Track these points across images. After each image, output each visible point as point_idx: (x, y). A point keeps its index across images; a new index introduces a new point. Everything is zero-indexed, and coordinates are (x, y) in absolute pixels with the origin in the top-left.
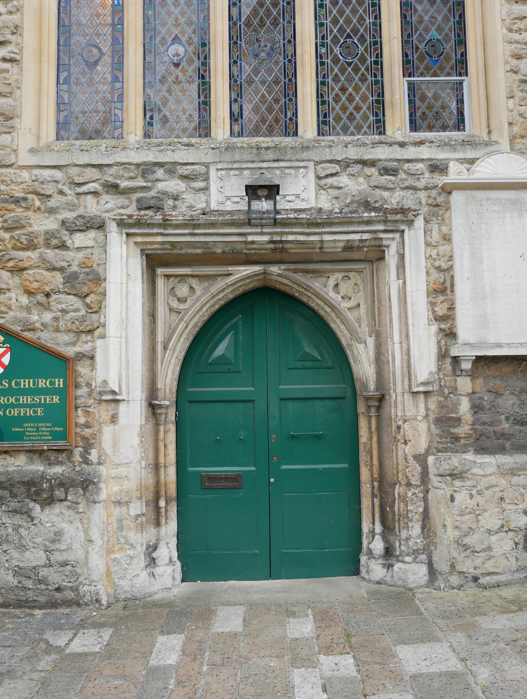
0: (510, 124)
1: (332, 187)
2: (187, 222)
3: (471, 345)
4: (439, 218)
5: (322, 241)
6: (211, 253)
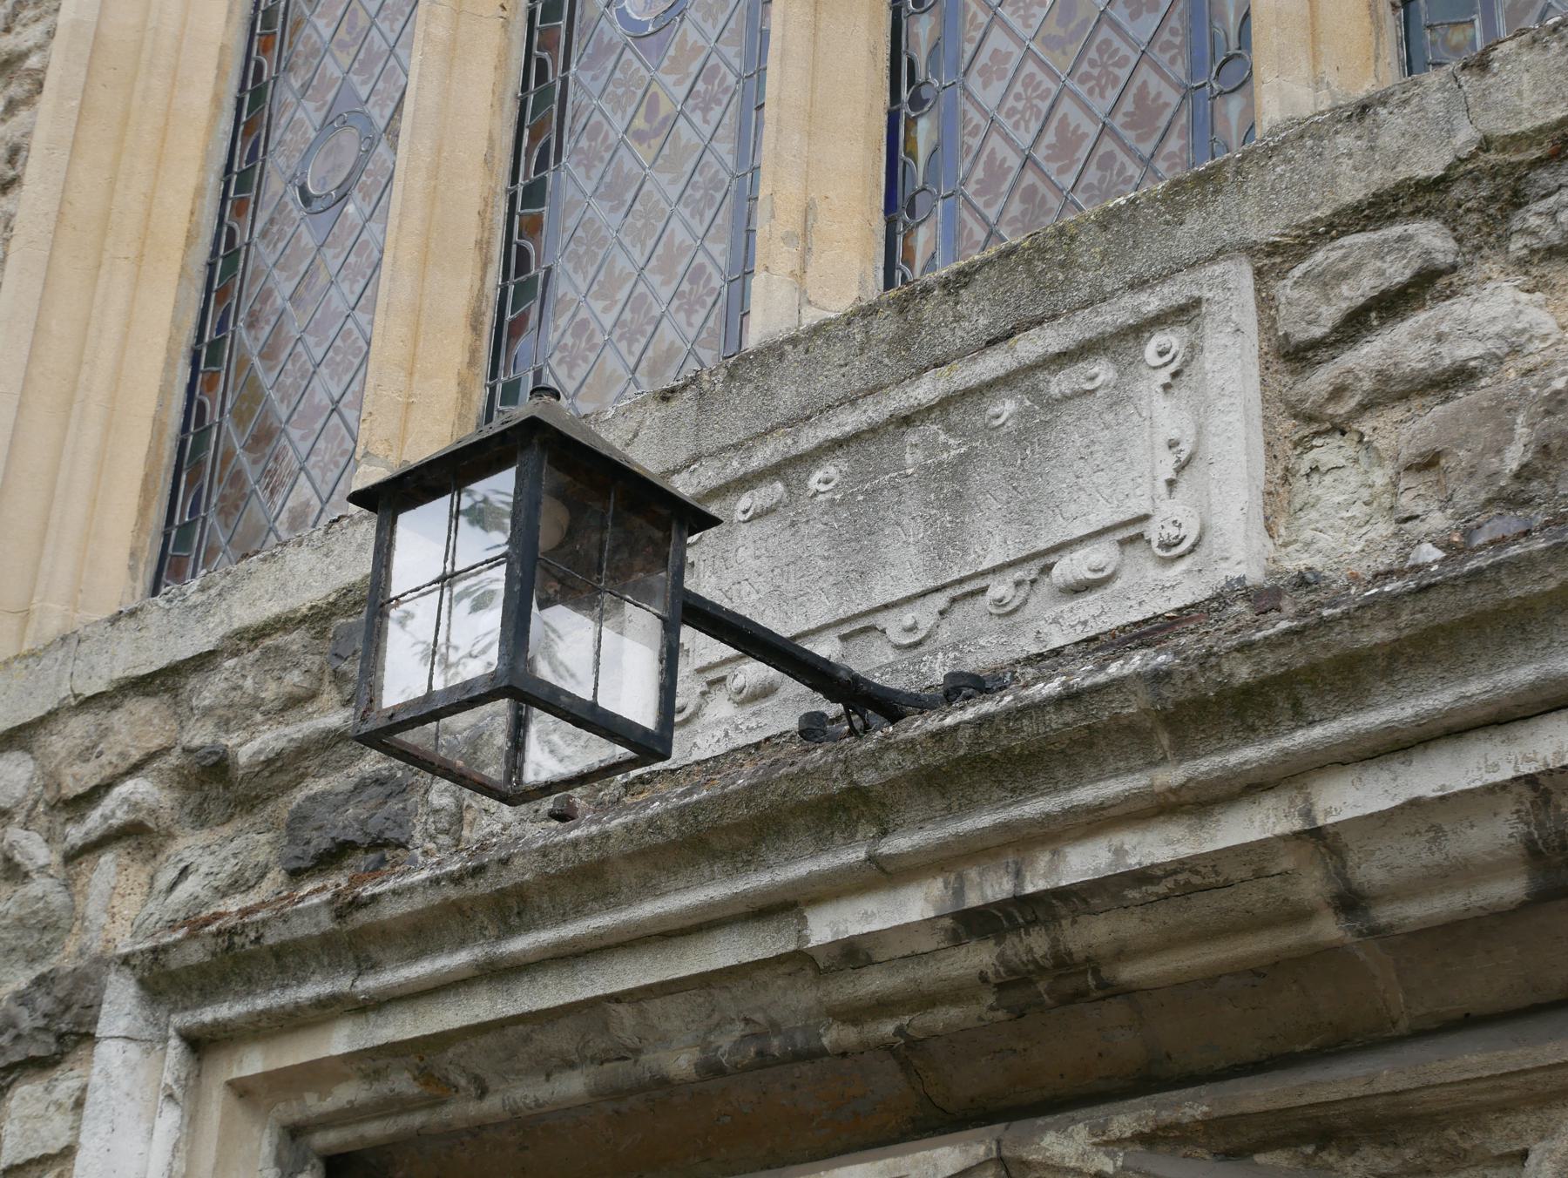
1: (1395, 391)
2: (452, 892)
5: (1317, 838)
6: (640, 1088)
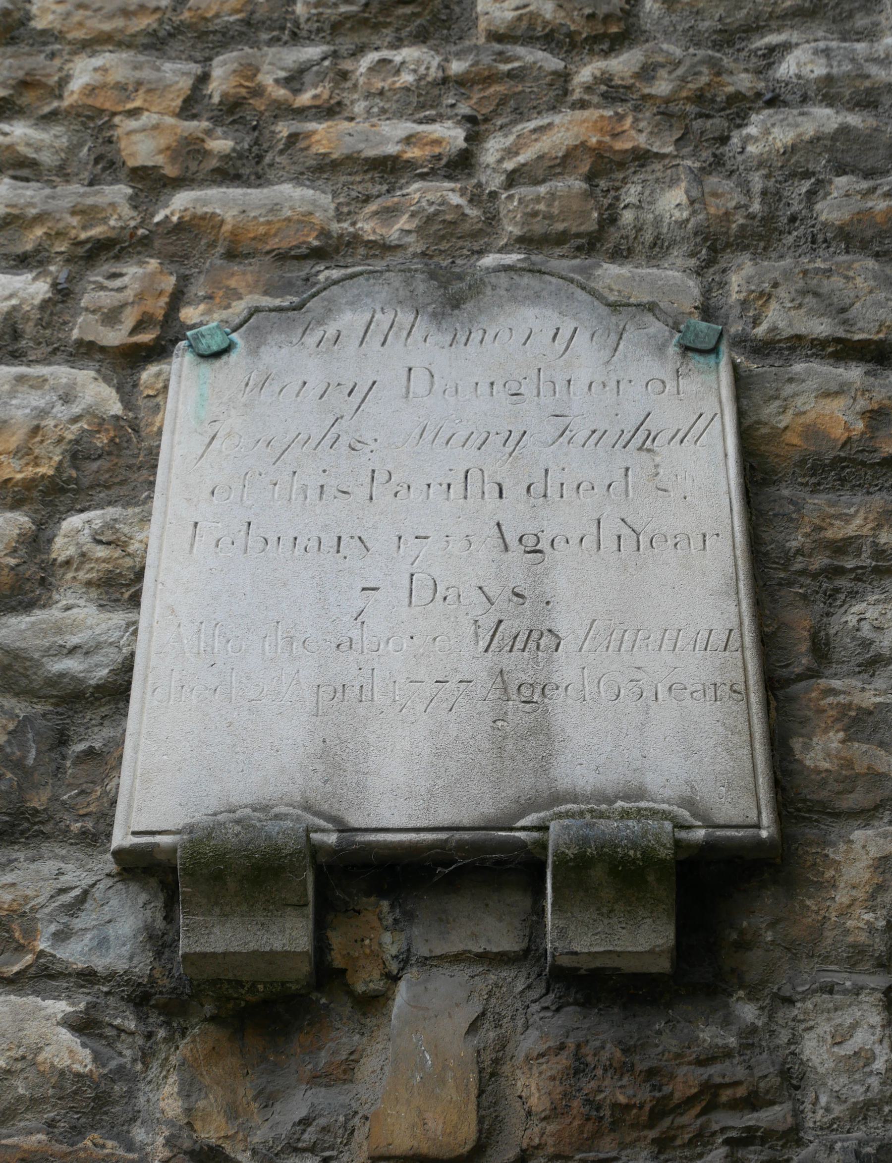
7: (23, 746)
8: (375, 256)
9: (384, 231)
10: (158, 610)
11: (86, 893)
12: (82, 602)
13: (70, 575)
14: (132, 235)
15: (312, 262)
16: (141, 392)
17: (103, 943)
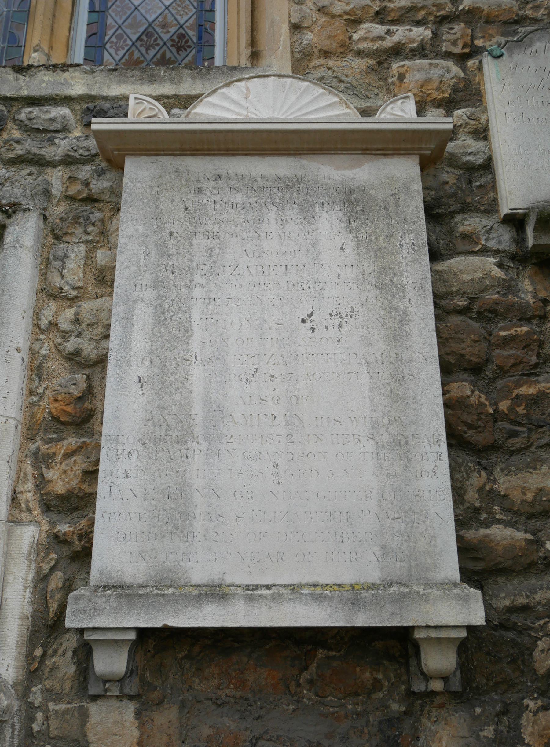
0: (296, 27)
3: (123, 591)
4: (90, 229)
7: (461, 183)
8: (533, 23)
9: (535, 14)
10: (500, 141)
11: (492, 227)
12: (468, 138)
13: (461, 130)
14: (455, 14)
15: (515, 25)
16: (469, 70)
17: (500, 242)
